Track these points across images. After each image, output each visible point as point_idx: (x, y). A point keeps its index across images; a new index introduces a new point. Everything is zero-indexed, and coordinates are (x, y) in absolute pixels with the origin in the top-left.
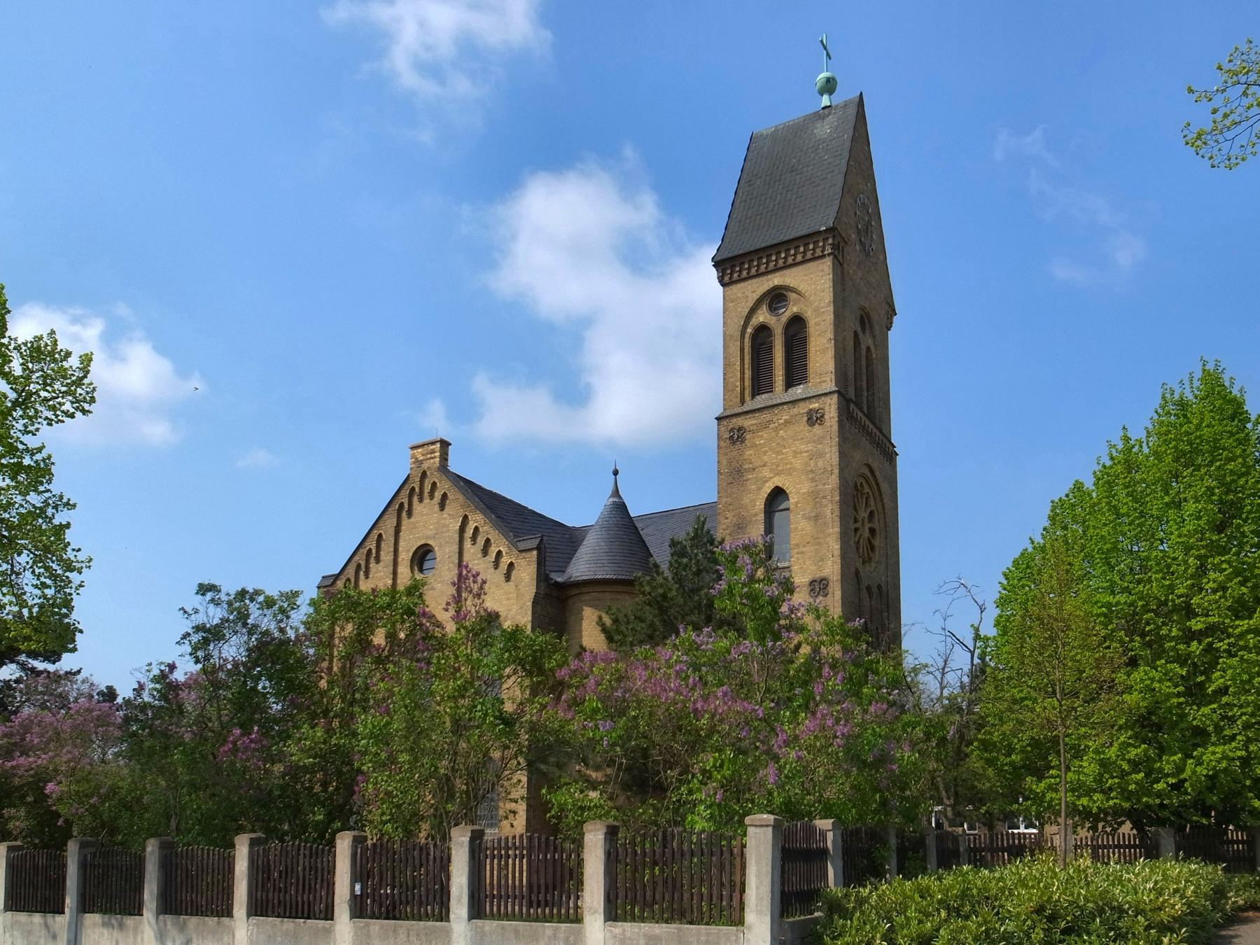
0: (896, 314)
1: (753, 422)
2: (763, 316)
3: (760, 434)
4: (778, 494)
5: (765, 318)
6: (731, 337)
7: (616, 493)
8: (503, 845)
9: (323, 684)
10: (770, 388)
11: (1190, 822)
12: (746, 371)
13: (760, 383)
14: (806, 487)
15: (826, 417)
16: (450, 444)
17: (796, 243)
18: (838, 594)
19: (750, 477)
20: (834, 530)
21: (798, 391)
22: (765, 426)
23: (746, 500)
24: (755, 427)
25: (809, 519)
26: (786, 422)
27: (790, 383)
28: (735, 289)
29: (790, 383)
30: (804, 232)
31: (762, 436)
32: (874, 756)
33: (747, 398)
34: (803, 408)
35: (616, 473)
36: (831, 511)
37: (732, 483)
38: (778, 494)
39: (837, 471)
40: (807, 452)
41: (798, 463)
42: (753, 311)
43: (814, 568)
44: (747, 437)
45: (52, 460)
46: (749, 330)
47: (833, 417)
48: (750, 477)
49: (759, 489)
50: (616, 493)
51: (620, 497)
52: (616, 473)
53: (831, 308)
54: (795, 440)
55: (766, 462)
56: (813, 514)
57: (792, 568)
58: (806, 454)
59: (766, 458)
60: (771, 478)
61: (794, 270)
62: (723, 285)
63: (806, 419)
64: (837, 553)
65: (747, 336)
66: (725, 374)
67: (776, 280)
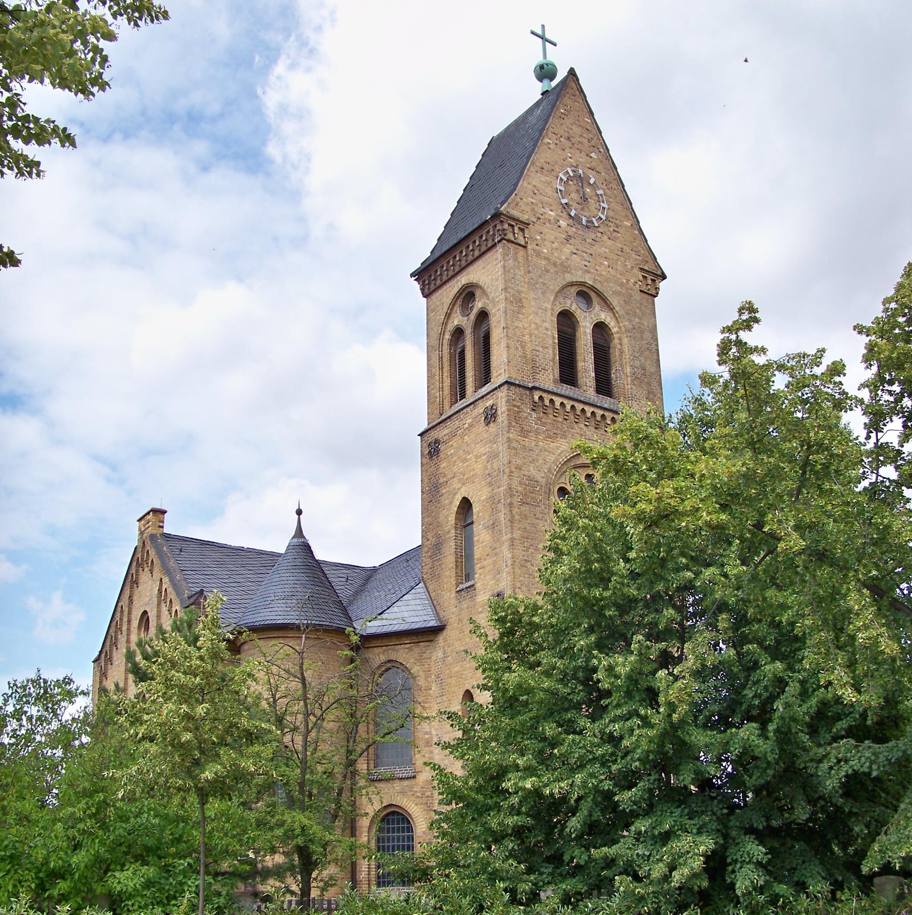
0: (664, 277)
1: (446, 432)
2: (458, 319)
3: (451, 443)
4: (466, 504)
5: (459, 321)
6: (432, 347)
7: (299, 532)
9: (854, 700)
10: (463, 396)
11: (846, 854)
12: (445, 379)
13: (459, 391)
14: (484, 494)
15: (499, 412)
16: (164, 512)
17: (472, 238)
19: (444, 491)
22: (453, 435)
23: (442, 518)
24: (446, 437)
25: (487, 528)
26: (471, 425)
27: (477, 388)
28: (434, 297)
29: (477, 388)
31: (452, 446)
32: (859, 770)
33: (447, 406)
34: (480, 408)
35: (299, 512)
37: (431, 501)
38: (466, 504)
40: (485, 454)
41: (479, 468)
42: (448, 316)
44: (442, 449)
46: (447, 336)
47: (504, 412)
48: (444, 491)
49: (451, 503)
50: (299, 532)
51: (304, 537)
52: (299, 512)
54: (476, 444)
55: (455, 473)
56: (491, 522)
57: (476, 586)
58: (486, 456)
59: (455, 469)
60: (459, 489)
61: (471, 269)
62: (426, 296)
63: (483, 418)
65: (446, 342)
66: (428, 387)
67: (463, 280)
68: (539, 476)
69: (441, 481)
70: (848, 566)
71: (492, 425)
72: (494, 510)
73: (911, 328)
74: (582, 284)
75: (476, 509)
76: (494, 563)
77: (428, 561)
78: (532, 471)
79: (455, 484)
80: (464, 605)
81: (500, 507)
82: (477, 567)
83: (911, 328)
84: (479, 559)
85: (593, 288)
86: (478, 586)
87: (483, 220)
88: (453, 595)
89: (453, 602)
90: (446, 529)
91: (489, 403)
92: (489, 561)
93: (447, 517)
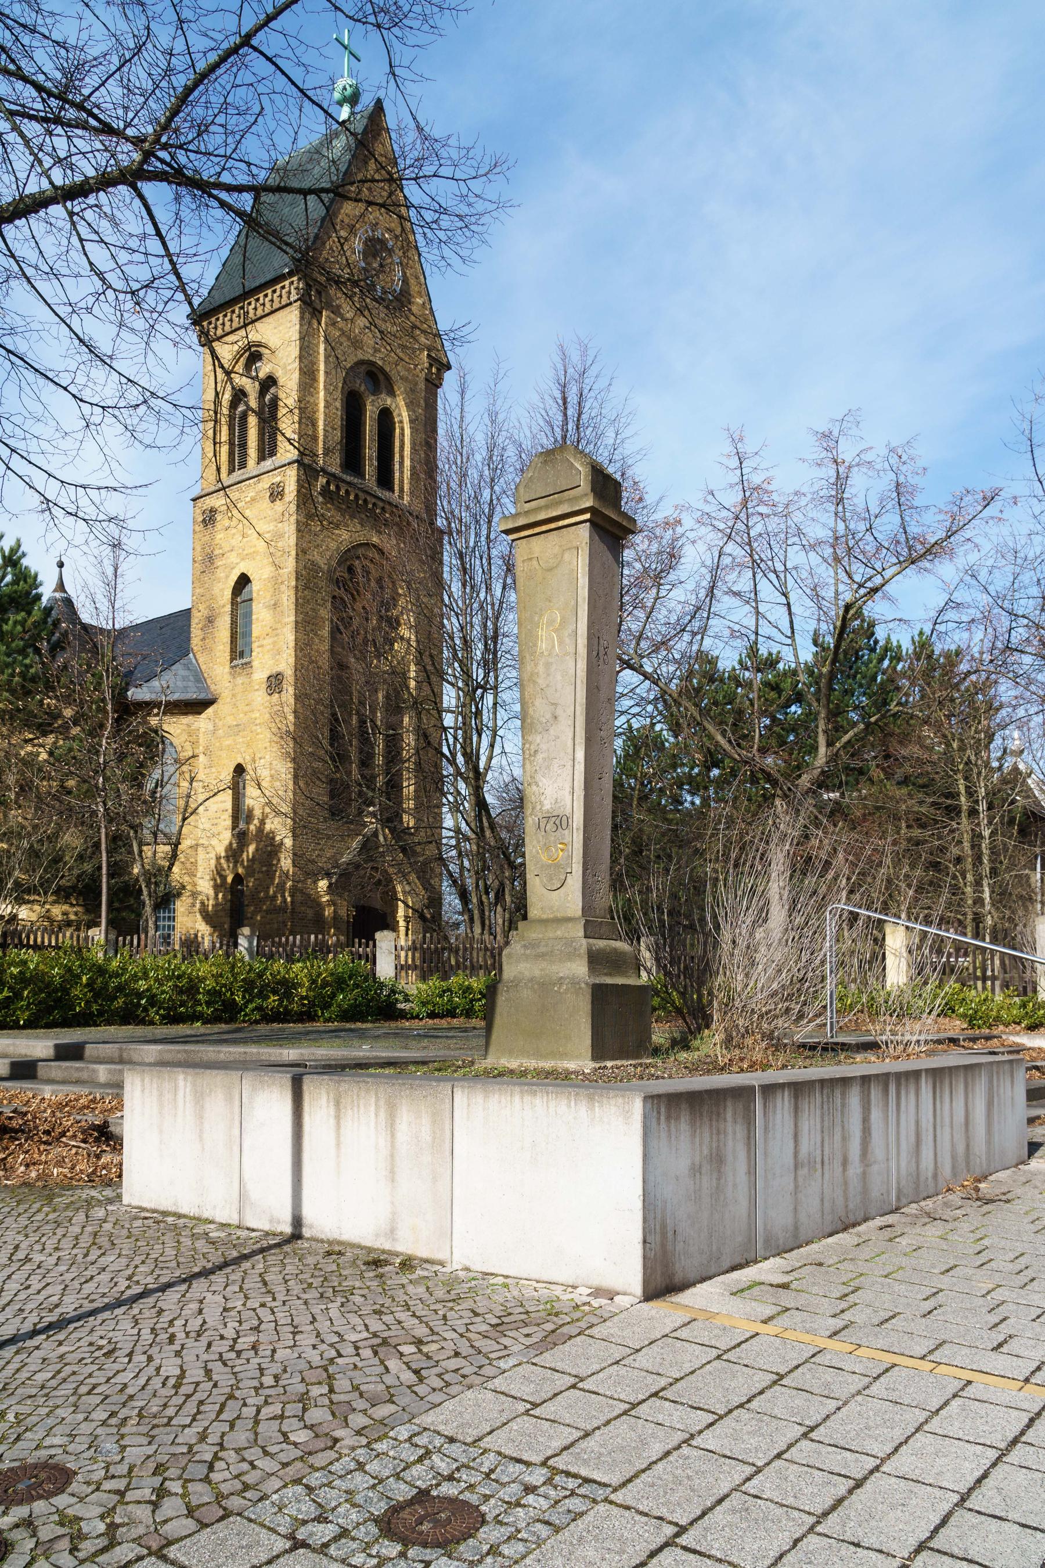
4: (243, 581)
8: (989, 983)
10: (243, 465)
15: (287, 491)
18: (291, 690)
20: (290, 618)
21: (268, 464)
23: (216, 591)
26: (253, 500)
27: (262, 458)
29: (262, 458)
30: (269, 277)
34: (266, 482)
35: (61, 565)
36: (288, 599)
38: (243, 581)
39: (293, 553)
43: (271, 662)
45: (951, 499)
49: (227, 577)
51: (65, 592)
52: (61, 565)
53: (297, 364)
64: (292, 644)
68: (322, 562)
69: (216, 552)
70: (906, 1020)
71: (278, 502)
72: (276, 591)
73: (1, 908)
74: (373, 364)
75: (256, 586)
76: (274, 643)
77: (199, 632)
78: (317, 558)
79: (232, 558)
80: (240, 680)
81: (283, 588)
82: (254, 646)
83: (1, 908)
84: (258, 638)
85: (381, 370)
86: (255, 664)
87: (279, 273)
88: (227, 669)
89: (227, 677)
90: (222, 603)
91: (278, 479)
92: (267, 641)
93: (222, 590)
